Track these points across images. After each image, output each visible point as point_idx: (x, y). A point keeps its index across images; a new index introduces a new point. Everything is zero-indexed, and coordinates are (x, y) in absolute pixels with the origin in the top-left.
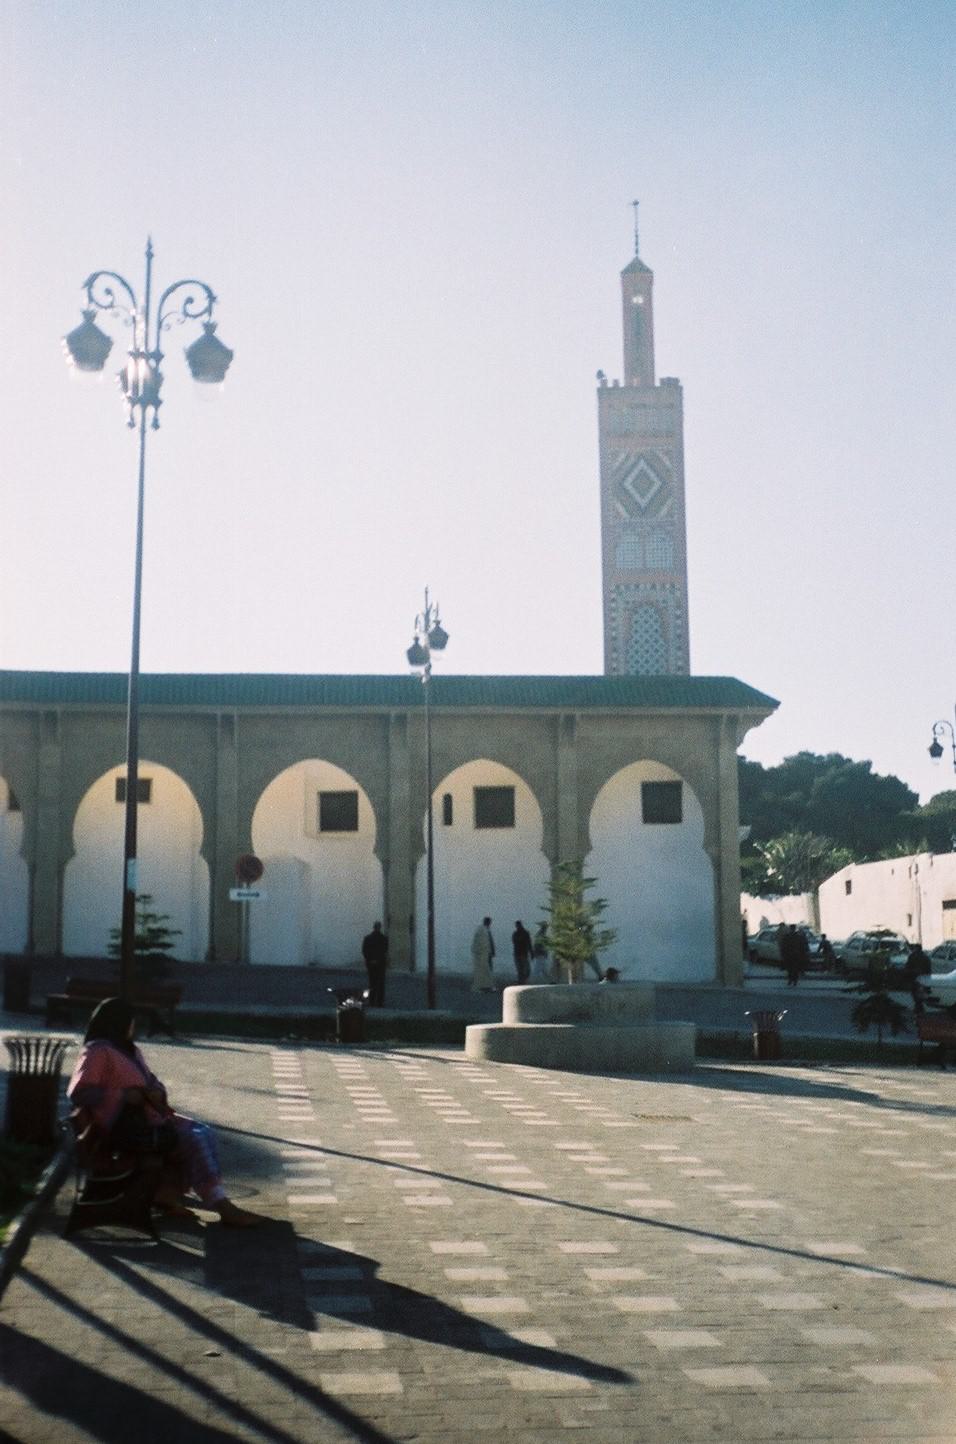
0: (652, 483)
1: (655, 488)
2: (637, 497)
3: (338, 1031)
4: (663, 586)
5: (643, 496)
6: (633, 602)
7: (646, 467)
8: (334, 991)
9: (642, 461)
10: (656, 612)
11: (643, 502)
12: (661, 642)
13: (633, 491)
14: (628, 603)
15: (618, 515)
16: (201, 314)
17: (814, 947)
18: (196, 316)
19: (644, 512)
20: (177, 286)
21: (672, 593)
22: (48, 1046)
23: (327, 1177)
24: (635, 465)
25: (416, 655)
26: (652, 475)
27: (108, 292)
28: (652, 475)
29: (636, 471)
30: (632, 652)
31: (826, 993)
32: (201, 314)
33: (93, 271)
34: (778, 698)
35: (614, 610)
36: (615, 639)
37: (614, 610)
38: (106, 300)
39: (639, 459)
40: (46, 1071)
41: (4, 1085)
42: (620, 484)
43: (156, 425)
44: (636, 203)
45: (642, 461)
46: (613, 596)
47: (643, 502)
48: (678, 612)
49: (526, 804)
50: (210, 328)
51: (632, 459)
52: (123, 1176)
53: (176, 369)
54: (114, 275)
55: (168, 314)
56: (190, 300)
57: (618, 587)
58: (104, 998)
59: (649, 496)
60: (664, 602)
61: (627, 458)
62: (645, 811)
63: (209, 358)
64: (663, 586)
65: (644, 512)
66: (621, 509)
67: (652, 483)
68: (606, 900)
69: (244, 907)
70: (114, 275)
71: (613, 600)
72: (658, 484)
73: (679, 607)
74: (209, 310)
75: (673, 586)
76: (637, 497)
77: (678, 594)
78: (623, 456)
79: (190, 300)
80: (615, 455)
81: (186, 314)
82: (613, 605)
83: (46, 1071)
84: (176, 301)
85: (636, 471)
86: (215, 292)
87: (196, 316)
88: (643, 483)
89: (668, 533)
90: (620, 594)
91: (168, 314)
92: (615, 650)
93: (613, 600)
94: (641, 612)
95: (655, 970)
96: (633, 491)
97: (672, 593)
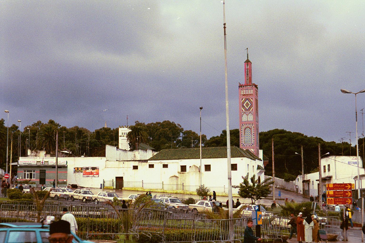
1: (250, 105)
2: (246, 107)
3: (345, 190)
5: (247, 107)
8: (249, 193)
11: (247, 108)
21: (252, 125)
22: (8, 207)
23: (46, 217)
26: (249, 103)
28: (249, 103)
30: (245, 136)
34: (185, 165)
41: (1, 191)
47: (247, 108)
57: (242, 124)
62: (210, 166)
64: (251, 124)
66: (243, 110)
71: (242, 127)
72: (244, 105)
75: (253, 124)
76: (246, 107)
89: (252, 114)
93: (242, 127)
94: (247, 129)
96: (245, 106)
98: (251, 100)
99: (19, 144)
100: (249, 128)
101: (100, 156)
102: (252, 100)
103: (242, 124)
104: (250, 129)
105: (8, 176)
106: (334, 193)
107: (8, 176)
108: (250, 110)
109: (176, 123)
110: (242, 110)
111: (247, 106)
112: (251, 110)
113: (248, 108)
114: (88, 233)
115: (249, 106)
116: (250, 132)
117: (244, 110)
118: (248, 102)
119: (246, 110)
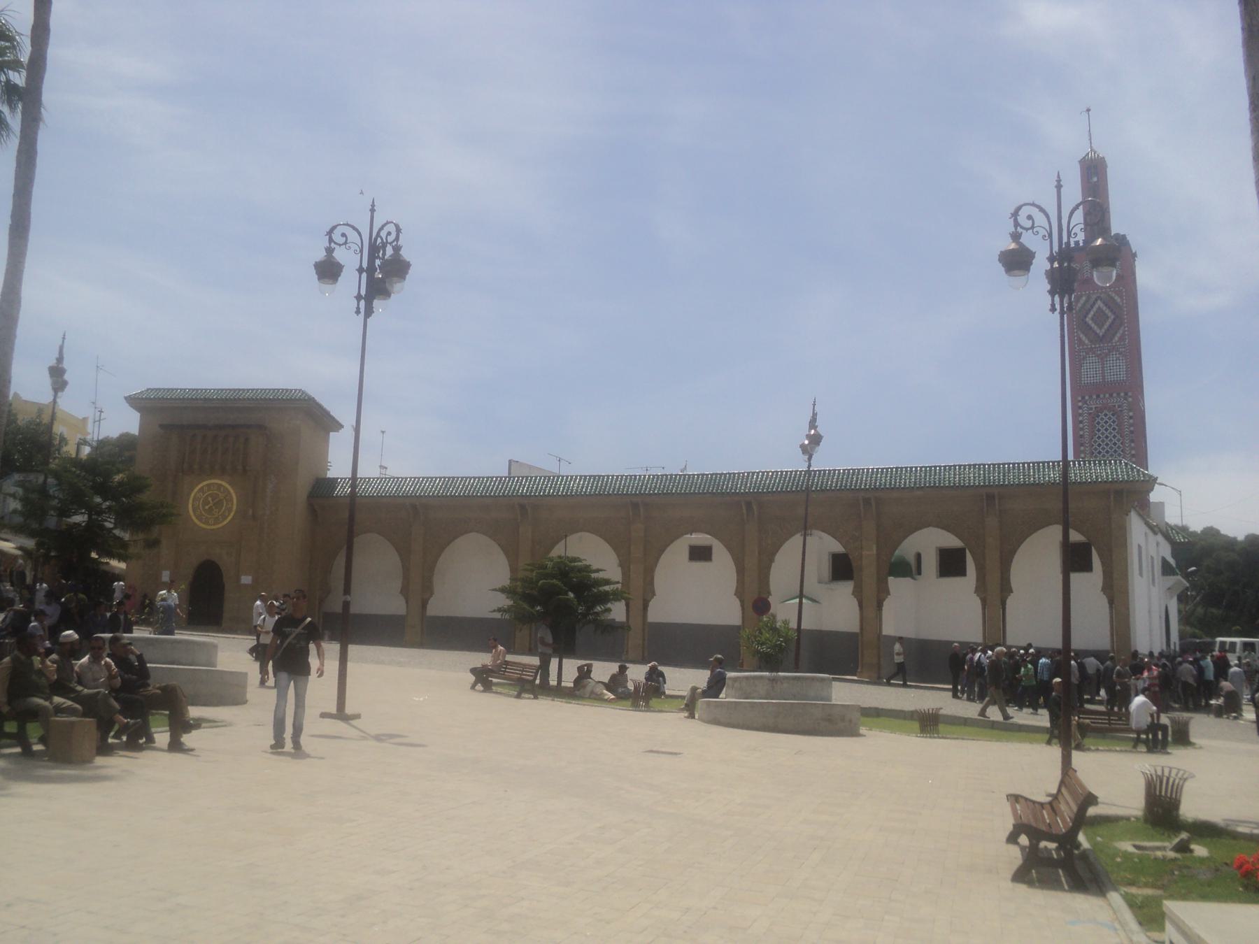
0: (1092, 319)
5: (1100, 329)
6: (1095, 408)
10: (1113, 415)
11: (1101, 332)
12: (1118, 436)
14: (1091, 409)
17: (254, 655)
19: (1102, 339)
24: (1094, 303)
25: (808, 451)
26: (1107, 311)
27: (1030, 217)
28: (1107, 311)
29: (1095, 309)
30: (1096, 446)
33: (1017, 205)
35: (1080, 415)
36: (1081, 436)
37: (1080, 415)
38: (1028, 224)
39: (1096, 300)
40: (292, 682)
44: (1088, 110)
46: (1080, 404)
47: (1101, 332)
49: (720, 551)
54: (1033, 205)
55: (1075, 226)
57: (1083, 398)
58: (720, 654)
59: (1106, 327)
60: (1119, 406)
65: (1102, 339)
66: (1084, 338)
67: (1092, 319)
70: (1033, 205)
75: (1126, 394)
82: (1080, 411)
83: (292, 682)
85: (1097, 306)
88: (1100, 318)
90: (1086, 403)
91: (1075, 226)
97: (1125, 399)
98: (1116, 298)
102: (1119, 300)
103: (1083, 398)
108: (1112, 340)
110: (1080, 339)
116: (1114, 426)
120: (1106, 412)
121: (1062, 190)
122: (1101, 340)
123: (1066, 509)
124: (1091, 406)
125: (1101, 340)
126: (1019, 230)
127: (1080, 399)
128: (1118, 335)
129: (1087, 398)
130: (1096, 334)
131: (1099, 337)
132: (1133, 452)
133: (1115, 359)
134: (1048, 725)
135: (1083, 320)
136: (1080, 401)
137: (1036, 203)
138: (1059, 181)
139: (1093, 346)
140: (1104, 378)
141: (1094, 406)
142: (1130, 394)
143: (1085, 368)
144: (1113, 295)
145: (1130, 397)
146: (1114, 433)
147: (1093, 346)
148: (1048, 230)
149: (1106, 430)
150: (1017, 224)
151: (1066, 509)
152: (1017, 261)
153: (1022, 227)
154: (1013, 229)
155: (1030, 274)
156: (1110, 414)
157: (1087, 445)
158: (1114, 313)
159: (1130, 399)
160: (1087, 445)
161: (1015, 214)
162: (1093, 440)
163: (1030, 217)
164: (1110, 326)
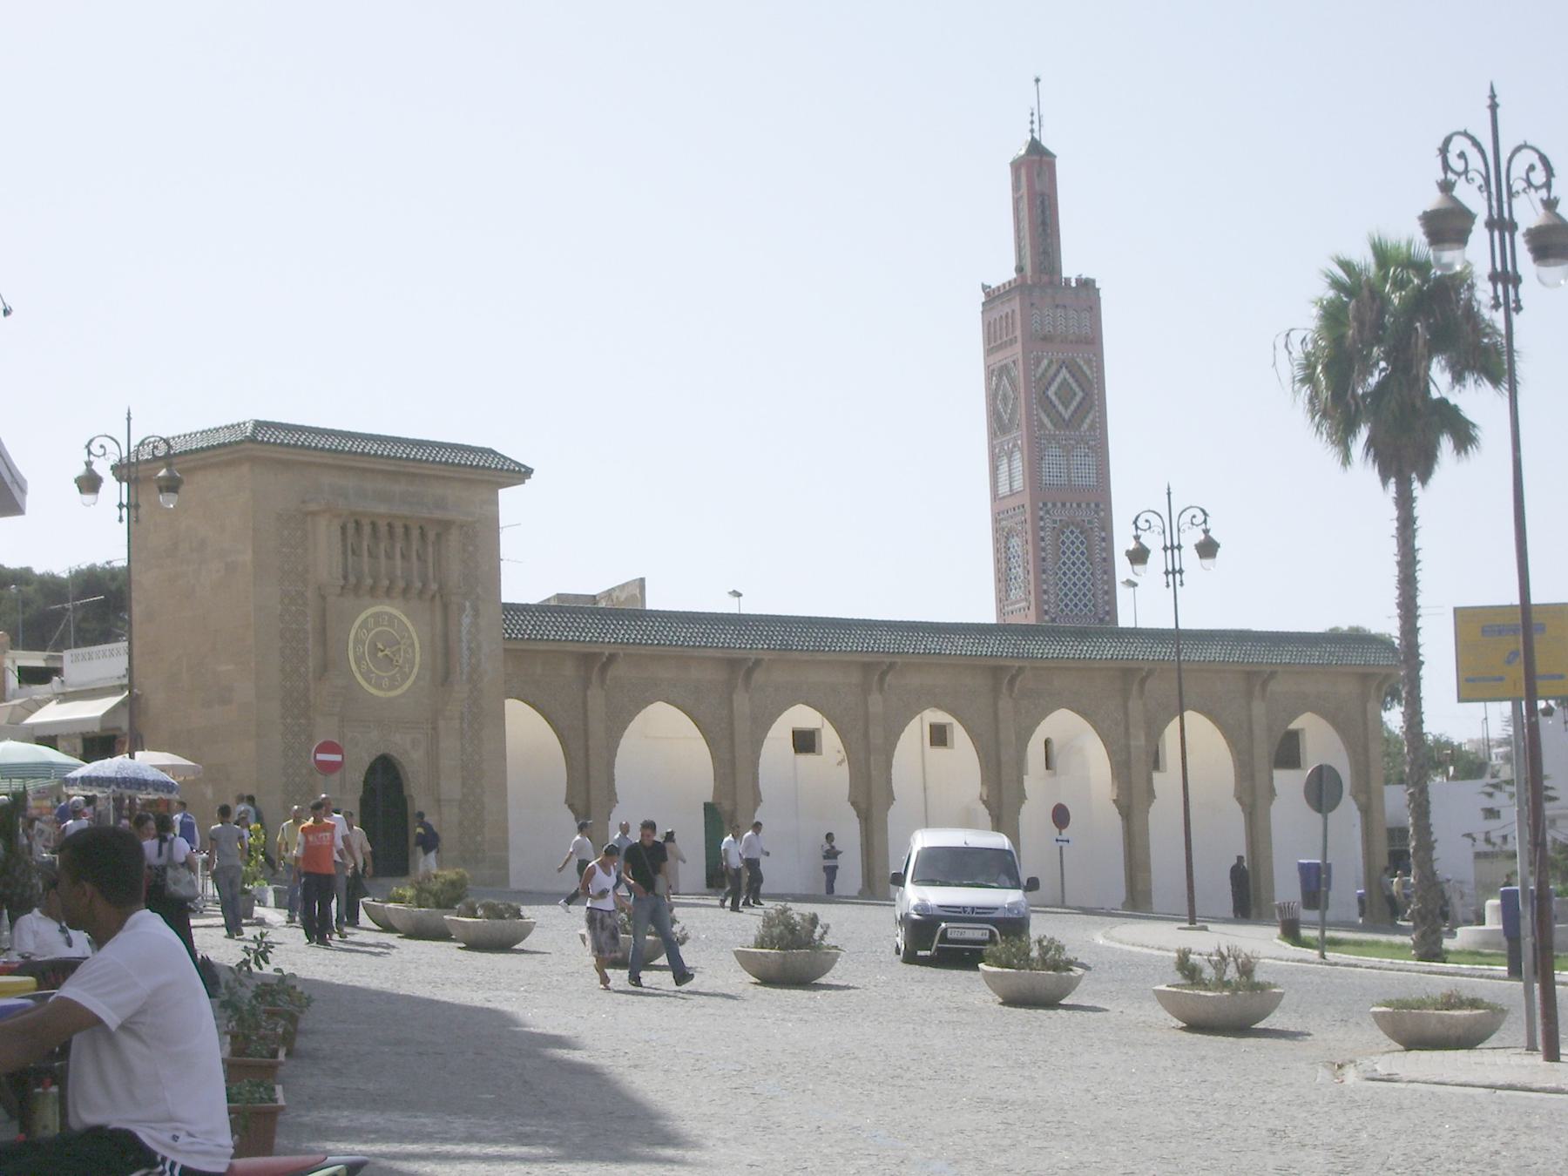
1: (1078, 399)
2: (1060, 408)
4: (1088, 505)
5: (1066, 408)
7: (1068, 376)
9: (1064, 369)
10: (1081, 533)
11: (1067, 415)
12: (1088, 564)
13: (1056, 402)
15: (1042, 425)
16: (1201, 524)
18: (1197, 526)
20: (1185, 510)
21: (1096, 512)
24: (1058, 372)
26: (1074, 385)
27: (1462, 155)
28: (1074, 385)
31: (396, 1119)
32: (1201, 524)
36: (1044, 559)
38: (101, 451)
42: (1044, 393)
43: (1182, 584)
45: (1064, 369)
46: (1041, 513)
47: (1067, 415)
48: (1103, 534)
50: (1206, 531)
51: (1054, 367)
52: (1209, 994)
53: (1189, 557)
56: (1194, 517)
57: (1045, 504)
61: (1049, 365)
63: (1208, 549)
64: (1088, 505)
66: (1046, 420)
67: (1075, 394)
68: (1552, 788)
69: (892, 903)
71: (1042, 519)
72: (1080, 395)
73: (1103, 529)
74: (1205, 521)
75: (1097, 505)
76: (1060, 408)
77: (1102, 514)
78: (1045, 362)
79: (1194, 517)
80: (1038, 362)
81: (1192, 524)
84: (1186, 517)
85: (1058, 380)
86: (1207, 512)
87: (1197, 526)
88: (1065, 394)
90: (1048, 512)
92: (1044, 572)
93: (1042, 519)
95: (310, 1098)
96: (1056, 402)
97: (1096, 512)
98: (1085, 368)
99: (1358, 959)
100: (1077, 526)
101: (814, 735)
102: (1088, 372)
103: (1045, 504)
104: (1063, 533)
105: (337, 758)
106: (1152, 775)
107: (337, 758)
108: (1080, 426)
109: (1418, 523)
110: (1040, 420)
111: (1063, 403)
112: (1085, 426)
113: (1072, 415)
114: (69, 605)
115: (1075, 404)
116: (1082, 548)
117: (1049, 425)
118: (1071, 380)
119: (1059, 422)
120: (1072, 528)
121: (1499, 111)
122: (1067, 426)
123: (27, 710)
124: (1054, 518)
125: (1067, 426)
126: (1451, 176)
127: (1041, 505)
128: (1088, 421)
129: (1050, 505)
130: (1061, 415)
131: (1064, 420)
132: (1045, 597)
133: (1083, 454)
134: (1557, 987)
135: (1087, 394)
136: (1041, 509)
137: (108, 434)
138: (1493, 97)
139: (1057, 432)
140: (1070, 481)
141: (1058, 519)
142: (1102, 506)
143: (1047, 462)
144: (1082, 363)
145: (1102, 510)
146: (1083, 559)
147: (1057, 432)
148: (1484, 173)
149: (1073, 553)
150: (1446, 166)
151: (27, 710)
152: (89, 483)
153: (1454, 172)
154: (1442, 176)
155: (99, 495)
156: (1077, 532)
157: (1051, 573)
158: (1083, 390)
159: (1102, 514)
160: (1051, 573)
161: (1444, 151)
162: (1057, 566)
163: (1462, 155)
164: (1078, 407)
